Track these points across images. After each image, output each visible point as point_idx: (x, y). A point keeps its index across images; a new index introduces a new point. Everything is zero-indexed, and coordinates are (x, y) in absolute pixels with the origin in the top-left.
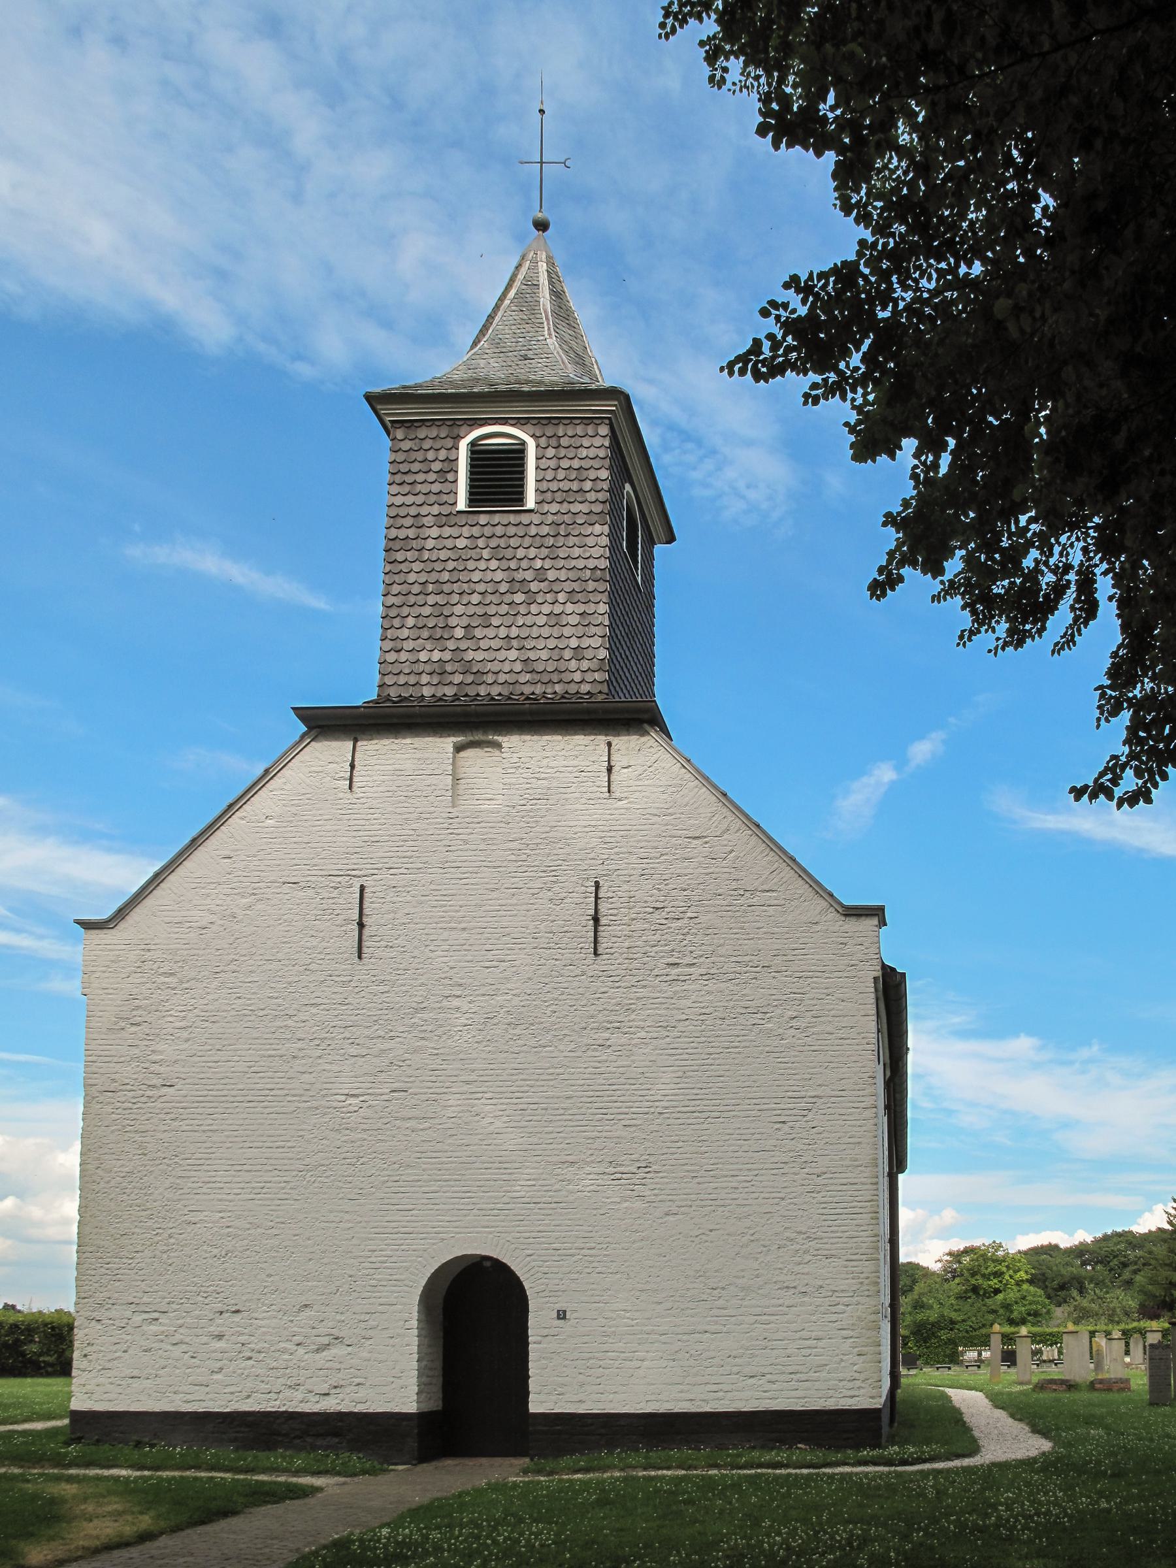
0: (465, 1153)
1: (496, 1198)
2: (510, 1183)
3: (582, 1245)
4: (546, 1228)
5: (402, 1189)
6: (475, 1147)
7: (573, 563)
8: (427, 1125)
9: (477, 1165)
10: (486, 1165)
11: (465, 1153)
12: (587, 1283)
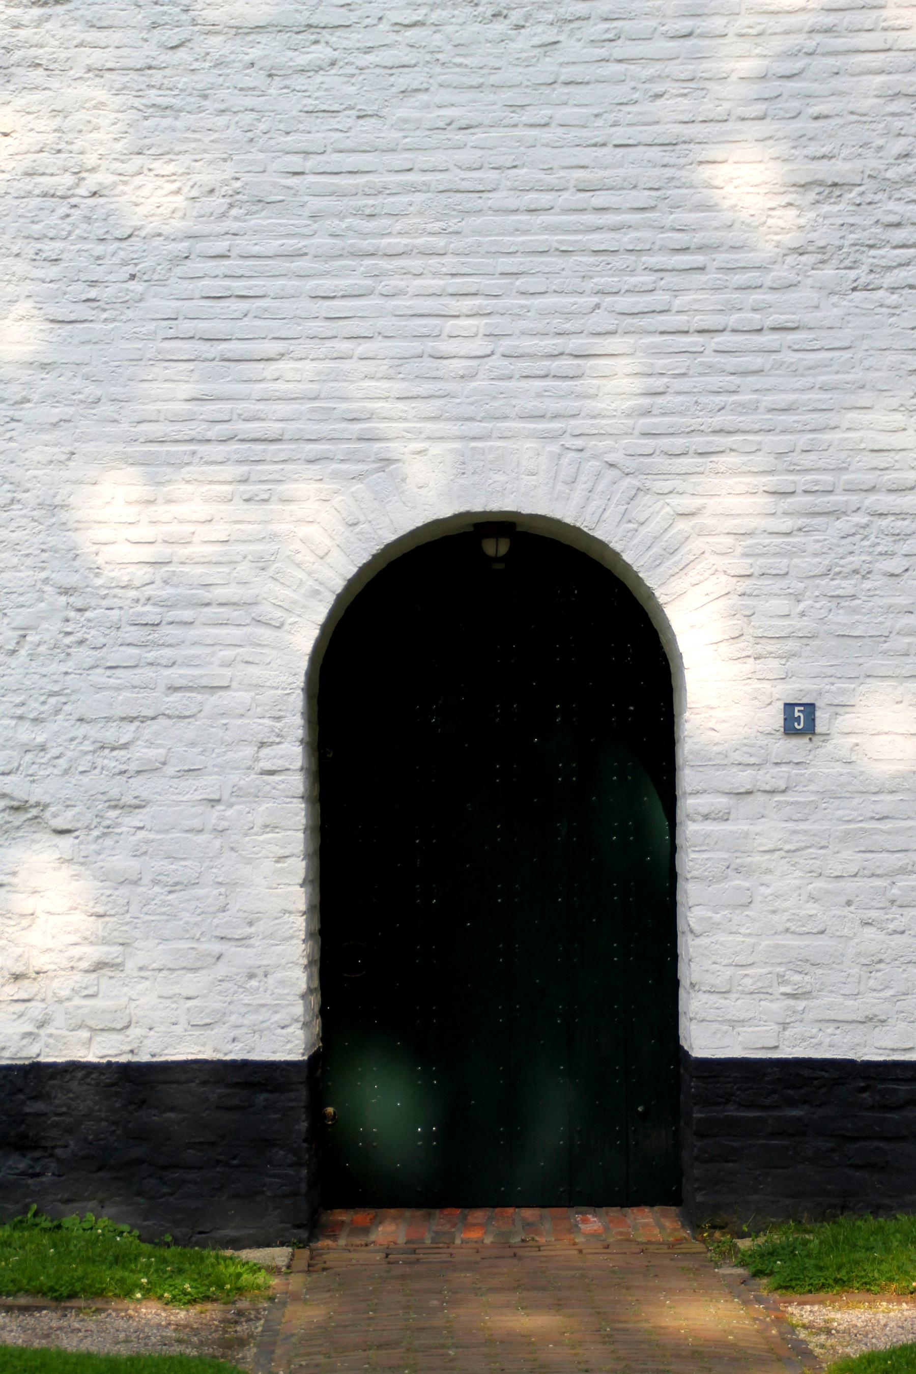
0: (461, 156)
1: (568, 315)
2: (618, 261)
3: (870, 478)
4: (745, 420)
5: (238, 286)
6: (494, 134)
7: (46, 182)
8: (320, 53)
9: (496, 199)
10: (529, 199)
11: (461, 156)
12: (889, 609)
